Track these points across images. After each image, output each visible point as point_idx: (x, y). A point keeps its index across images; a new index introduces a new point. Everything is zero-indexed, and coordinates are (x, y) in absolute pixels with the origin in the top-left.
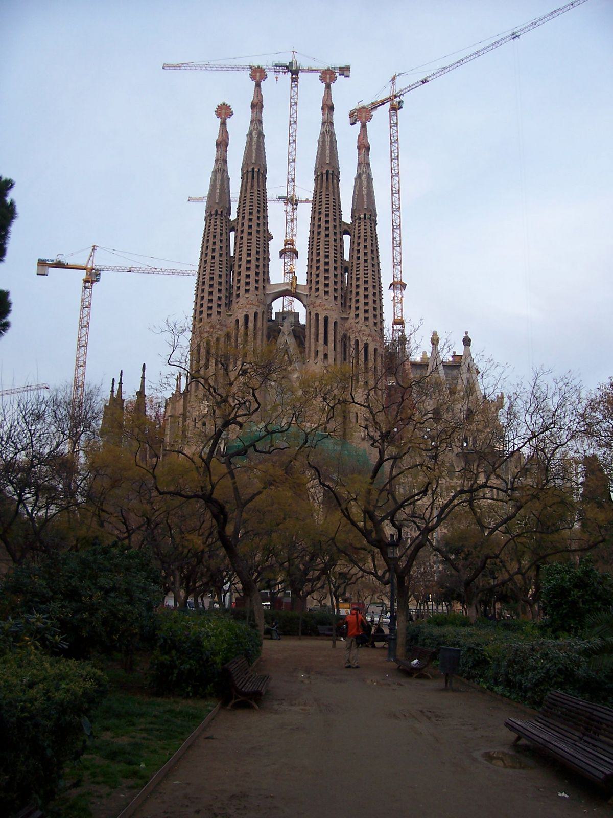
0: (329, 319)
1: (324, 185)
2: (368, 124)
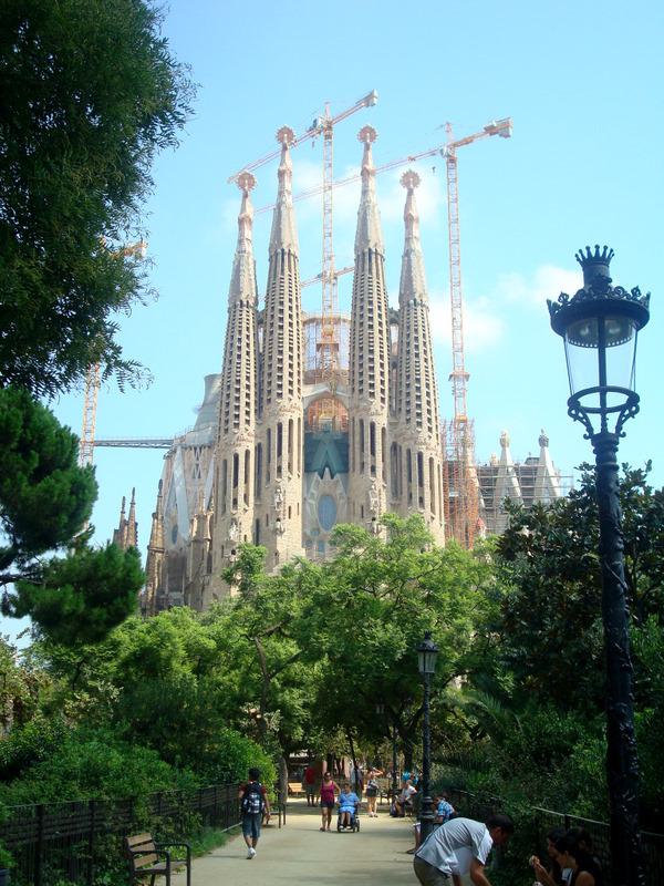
0: (377, 425)
1: (367, 267)
2: (497, 135)
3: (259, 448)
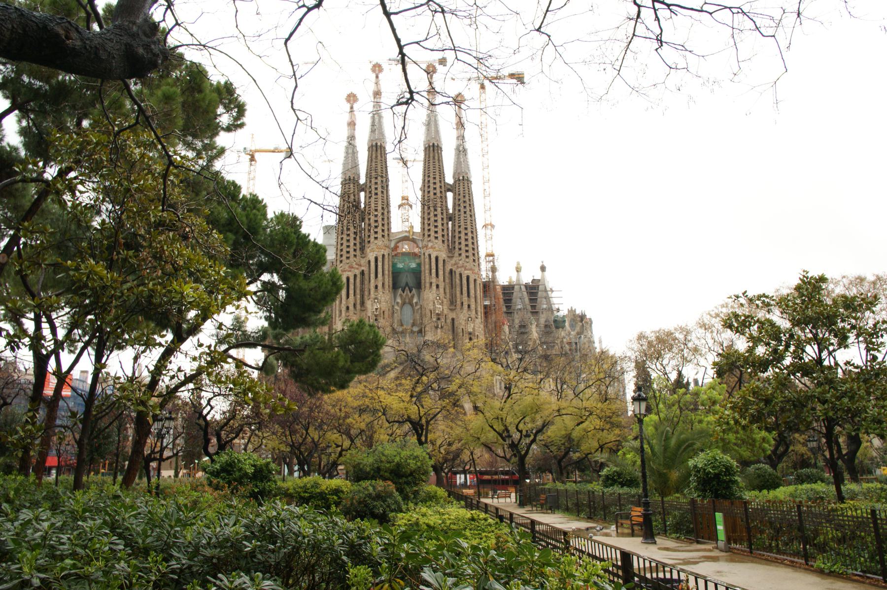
3: (363, 273)
